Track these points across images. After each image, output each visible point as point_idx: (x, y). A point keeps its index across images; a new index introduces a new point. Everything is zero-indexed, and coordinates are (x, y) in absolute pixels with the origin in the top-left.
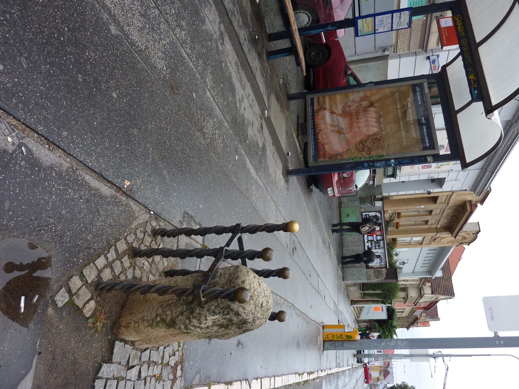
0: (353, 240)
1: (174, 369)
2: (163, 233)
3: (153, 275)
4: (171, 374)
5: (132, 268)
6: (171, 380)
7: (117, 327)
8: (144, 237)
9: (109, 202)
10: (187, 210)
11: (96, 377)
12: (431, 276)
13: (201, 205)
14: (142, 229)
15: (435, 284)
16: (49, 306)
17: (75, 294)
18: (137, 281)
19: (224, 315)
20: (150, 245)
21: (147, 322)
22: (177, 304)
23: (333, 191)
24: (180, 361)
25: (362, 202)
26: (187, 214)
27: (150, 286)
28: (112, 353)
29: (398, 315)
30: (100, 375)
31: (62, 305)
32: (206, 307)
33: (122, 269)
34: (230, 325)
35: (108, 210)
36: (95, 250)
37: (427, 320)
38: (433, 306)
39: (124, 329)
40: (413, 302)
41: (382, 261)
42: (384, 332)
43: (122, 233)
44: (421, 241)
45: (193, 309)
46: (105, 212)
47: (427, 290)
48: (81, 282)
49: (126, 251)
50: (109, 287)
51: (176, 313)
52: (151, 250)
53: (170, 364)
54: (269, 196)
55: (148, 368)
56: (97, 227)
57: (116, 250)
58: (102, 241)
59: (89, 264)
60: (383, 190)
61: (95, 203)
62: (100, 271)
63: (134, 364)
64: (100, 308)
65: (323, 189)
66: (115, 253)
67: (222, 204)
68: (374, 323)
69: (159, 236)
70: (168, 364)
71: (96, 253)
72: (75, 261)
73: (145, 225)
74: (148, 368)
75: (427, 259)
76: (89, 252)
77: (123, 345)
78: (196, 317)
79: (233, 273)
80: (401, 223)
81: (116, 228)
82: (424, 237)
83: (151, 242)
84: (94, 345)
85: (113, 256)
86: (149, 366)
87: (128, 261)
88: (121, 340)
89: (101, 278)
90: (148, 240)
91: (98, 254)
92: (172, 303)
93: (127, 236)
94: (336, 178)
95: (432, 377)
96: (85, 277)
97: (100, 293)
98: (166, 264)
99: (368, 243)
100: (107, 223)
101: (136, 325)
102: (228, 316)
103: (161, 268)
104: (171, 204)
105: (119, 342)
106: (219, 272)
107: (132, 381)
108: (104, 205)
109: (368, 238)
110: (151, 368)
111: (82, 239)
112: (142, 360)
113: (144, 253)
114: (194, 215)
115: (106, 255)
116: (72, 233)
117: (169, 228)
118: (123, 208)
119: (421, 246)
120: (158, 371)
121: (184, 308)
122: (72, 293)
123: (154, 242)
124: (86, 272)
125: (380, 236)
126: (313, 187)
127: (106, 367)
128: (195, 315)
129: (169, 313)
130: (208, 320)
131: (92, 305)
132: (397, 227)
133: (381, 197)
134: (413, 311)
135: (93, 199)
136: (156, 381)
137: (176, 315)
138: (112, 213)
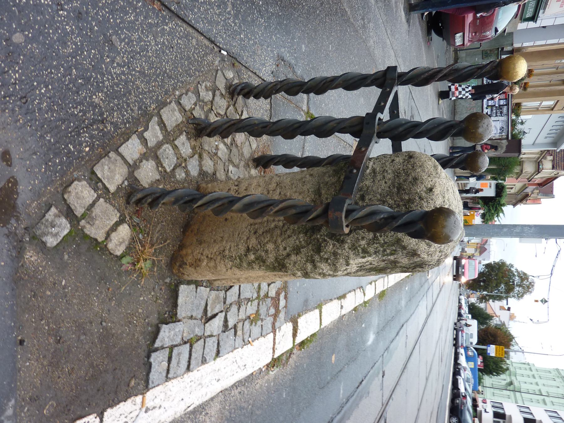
0: (468, 106)
1: (276, 300)
2: (246, 91)
3: (234, 166)
4: (271, 308)
5: (196, 156)
6: (271, 316)
7: (178, 264)
8: (213, 98)
9: (133, 22)
10: (283, 53)
11: (151, 350)
12: (556, 149)
13: (303, 46)
14: (208, 84)
15: (558, 158)
16: (25, 248)
17: (83, 216)
18: (209, 179)
19: (384, 256)
20: (226, 113)
21: (231, 261)
22: (286, 231)
23: (462, 38)
24: (282, 287)
25: (484, 57)
26: (282, 60)
27: (231, 199)
28: (175, 305)
29: (508, 191)
30: (158, 344)
31: (55, 243)
32: (349, 241)
33: (178, 158)
34: (389, 268)
35: (133, 41)
36: (115, 125)
37: (539, 197)
38: (550, 182)
39: (190, 268)
40: (527, 177)
41: (503, 131)
42: (489, 210)
43: (171, 90)
44: (553, 106)
45: (320, 244)
46: (128, 44)
47: (547, 164)
48: (93, 191)
49: (181, 126)
50: (150, 200)
51: (285, 249)
52: (228, 122)
53: (269, 296)
54: (388, 41)
55: (239, 310)
56: (112, 76)
57: (162, 124)
58: (128, 106)
59: (107, 154)
60: (514, 40)
61: (99, 23)
62: (133, 167)
63: (216, 311)
64: (140, 236)
65: (448, 36)
66: (161, 130)
67: (333, 47)
68: (478, 201)
69: (240, 98)
70: (266, 296)
71: (119, 131)
72: (73, 149)
73: (214, 77)
74: (239, 310)
75: (554, 128)
76: (103, 130)
77: (193, 289)
78: (327, 259)
79: (404, 170)
80: (530, 84)
81: (155, 80)
82: (558, 101)
83: (227, 109)
84: (142, 298)
85: (157, 137)
86: (240, 307)
87: (188, 145)
88: (189, 283)
89: (136, 179)
90: (221, 104)
91: (123, 134)
92: (276, 227)
93: (181, 96)
94: (470, 18)
95: (536, 256)
96: (100, 181)
97: (137, 209)
98: (254, 146)
99: (487, 108)
100: (134, 70)
101: (212, 264)
102: (392, 258)
103: (247, 152)
104: (256, 38)
105: (185, 286)
106: (370, 167)
107: (214, 336)
108: (121, 29)
109: (487, 103)
110: (242, 309)
111: (81, 103)
112: (228, 301)
113: (216, 128)
114: (293, 62)
115: (142, 134)
116: (52, 89)
117: (256, 82)
118: (167, 40)
119: (551, 112)
120: (253, 309)
121: (301, 240)
122: (77, 217)
123: (231, 108)
124: (103, 171)
125: (504, 100)
126: (434, 35)
127: (167, 330)
128: (326, 256)
129: (270, 246)
130: (351, 265)
131: (124, 232)
132: (525, 88)
133: (511, 49)
134: (524, 187)
135: (92, 12)
136: (251, 324)
137: (285, 253)
138: (143, 49)
